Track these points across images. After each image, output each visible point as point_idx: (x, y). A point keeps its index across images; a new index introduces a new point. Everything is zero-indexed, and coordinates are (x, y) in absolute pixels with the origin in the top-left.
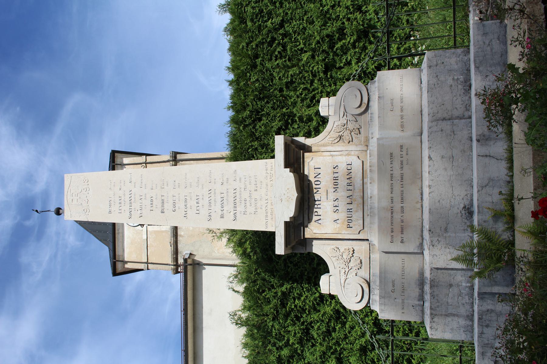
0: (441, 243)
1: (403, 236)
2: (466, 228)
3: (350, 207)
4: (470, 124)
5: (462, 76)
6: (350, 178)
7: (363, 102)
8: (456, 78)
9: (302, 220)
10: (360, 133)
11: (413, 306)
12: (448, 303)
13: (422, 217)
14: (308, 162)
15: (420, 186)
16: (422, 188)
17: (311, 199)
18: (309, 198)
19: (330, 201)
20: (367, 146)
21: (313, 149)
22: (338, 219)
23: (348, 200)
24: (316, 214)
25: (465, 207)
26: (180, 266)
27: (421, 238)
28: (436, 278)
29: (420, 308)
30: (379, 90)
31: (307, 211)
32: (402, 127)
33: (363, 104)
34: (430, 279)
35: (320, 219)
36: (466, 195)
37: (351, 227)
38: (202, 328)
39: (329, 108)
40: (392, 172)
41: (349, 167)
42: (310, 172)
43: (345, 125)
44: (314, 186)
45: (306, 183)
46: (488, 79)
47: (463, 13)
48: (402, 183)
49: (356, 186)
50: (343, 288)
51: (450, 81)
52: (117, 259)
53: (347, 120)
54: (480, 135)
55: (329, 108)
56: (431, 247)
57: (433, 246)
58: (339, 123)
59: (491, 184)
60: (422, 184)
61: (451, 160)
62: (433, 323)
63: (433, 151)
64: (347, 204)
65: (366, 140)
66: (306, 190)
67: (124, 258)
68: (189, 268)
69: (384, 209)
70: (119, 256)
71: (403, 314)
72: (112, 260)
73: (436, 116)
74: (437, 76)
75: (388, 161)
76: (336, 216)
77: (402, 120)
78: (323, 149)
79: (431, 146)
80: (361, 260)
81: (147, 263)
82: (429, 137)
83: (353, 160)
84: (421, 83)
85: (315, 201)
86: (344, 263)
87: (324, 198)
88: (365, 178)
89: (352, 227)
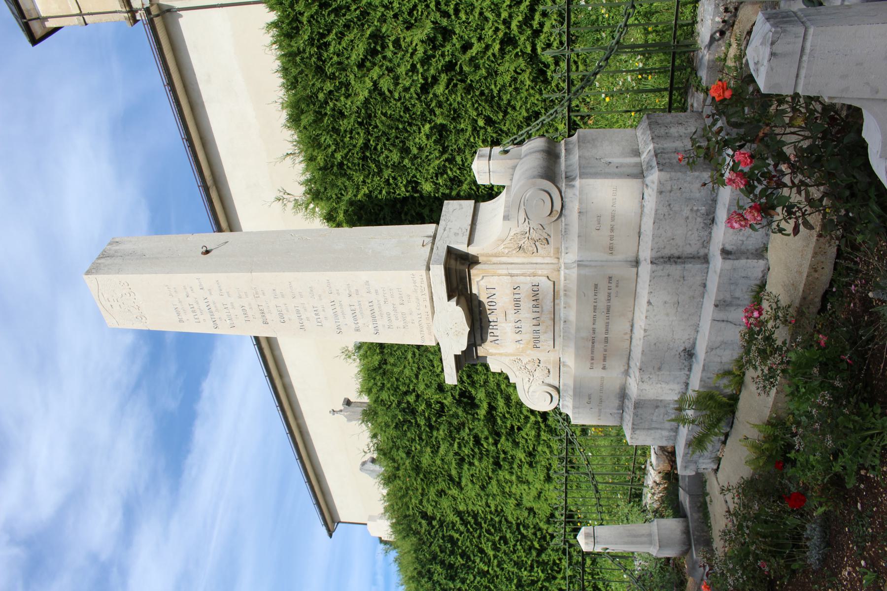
1: (605, 363)
2: (683, 366)
3: (537, 328)
4: (706, 270)
5: (703, 208)
8: (695, 208)
12: (652, 420)
13: (630, 346)
16: (633, 320)
17: (484, 320)
18: (481, 319)
20: (558, 258)
21: (481, 259)
23: (535, 322)
24: (492, 334)
25: (685, 350)
26: (137, 11)
29: (620, 416)
30: (580, 203)
31: (479, 331)
33: (554, 212)
36: (689, 339)
38: (203, 103)
40: (595, 304)
41: (535, 288)
44: (487, 307)
45: (475, 303)
46: (741, 233)
47: (807, 553)
49: (544, 308)
51: (686, 212)
52: (28, 17)
54: (720, 301)
58: (518, 230)
59: (723, 346)
61: (676, 305)
66: (476, 310)
67: (38, 13)
68: (157, 21)
70: (28, 11)
72: (19, 20)
74: (669, 205)
75: (591, 293)
76: (518, 337)
77: (612, 242)
78: (495, 260)
81: (81, 14)
82: (650, 281)
87: (501, 318)
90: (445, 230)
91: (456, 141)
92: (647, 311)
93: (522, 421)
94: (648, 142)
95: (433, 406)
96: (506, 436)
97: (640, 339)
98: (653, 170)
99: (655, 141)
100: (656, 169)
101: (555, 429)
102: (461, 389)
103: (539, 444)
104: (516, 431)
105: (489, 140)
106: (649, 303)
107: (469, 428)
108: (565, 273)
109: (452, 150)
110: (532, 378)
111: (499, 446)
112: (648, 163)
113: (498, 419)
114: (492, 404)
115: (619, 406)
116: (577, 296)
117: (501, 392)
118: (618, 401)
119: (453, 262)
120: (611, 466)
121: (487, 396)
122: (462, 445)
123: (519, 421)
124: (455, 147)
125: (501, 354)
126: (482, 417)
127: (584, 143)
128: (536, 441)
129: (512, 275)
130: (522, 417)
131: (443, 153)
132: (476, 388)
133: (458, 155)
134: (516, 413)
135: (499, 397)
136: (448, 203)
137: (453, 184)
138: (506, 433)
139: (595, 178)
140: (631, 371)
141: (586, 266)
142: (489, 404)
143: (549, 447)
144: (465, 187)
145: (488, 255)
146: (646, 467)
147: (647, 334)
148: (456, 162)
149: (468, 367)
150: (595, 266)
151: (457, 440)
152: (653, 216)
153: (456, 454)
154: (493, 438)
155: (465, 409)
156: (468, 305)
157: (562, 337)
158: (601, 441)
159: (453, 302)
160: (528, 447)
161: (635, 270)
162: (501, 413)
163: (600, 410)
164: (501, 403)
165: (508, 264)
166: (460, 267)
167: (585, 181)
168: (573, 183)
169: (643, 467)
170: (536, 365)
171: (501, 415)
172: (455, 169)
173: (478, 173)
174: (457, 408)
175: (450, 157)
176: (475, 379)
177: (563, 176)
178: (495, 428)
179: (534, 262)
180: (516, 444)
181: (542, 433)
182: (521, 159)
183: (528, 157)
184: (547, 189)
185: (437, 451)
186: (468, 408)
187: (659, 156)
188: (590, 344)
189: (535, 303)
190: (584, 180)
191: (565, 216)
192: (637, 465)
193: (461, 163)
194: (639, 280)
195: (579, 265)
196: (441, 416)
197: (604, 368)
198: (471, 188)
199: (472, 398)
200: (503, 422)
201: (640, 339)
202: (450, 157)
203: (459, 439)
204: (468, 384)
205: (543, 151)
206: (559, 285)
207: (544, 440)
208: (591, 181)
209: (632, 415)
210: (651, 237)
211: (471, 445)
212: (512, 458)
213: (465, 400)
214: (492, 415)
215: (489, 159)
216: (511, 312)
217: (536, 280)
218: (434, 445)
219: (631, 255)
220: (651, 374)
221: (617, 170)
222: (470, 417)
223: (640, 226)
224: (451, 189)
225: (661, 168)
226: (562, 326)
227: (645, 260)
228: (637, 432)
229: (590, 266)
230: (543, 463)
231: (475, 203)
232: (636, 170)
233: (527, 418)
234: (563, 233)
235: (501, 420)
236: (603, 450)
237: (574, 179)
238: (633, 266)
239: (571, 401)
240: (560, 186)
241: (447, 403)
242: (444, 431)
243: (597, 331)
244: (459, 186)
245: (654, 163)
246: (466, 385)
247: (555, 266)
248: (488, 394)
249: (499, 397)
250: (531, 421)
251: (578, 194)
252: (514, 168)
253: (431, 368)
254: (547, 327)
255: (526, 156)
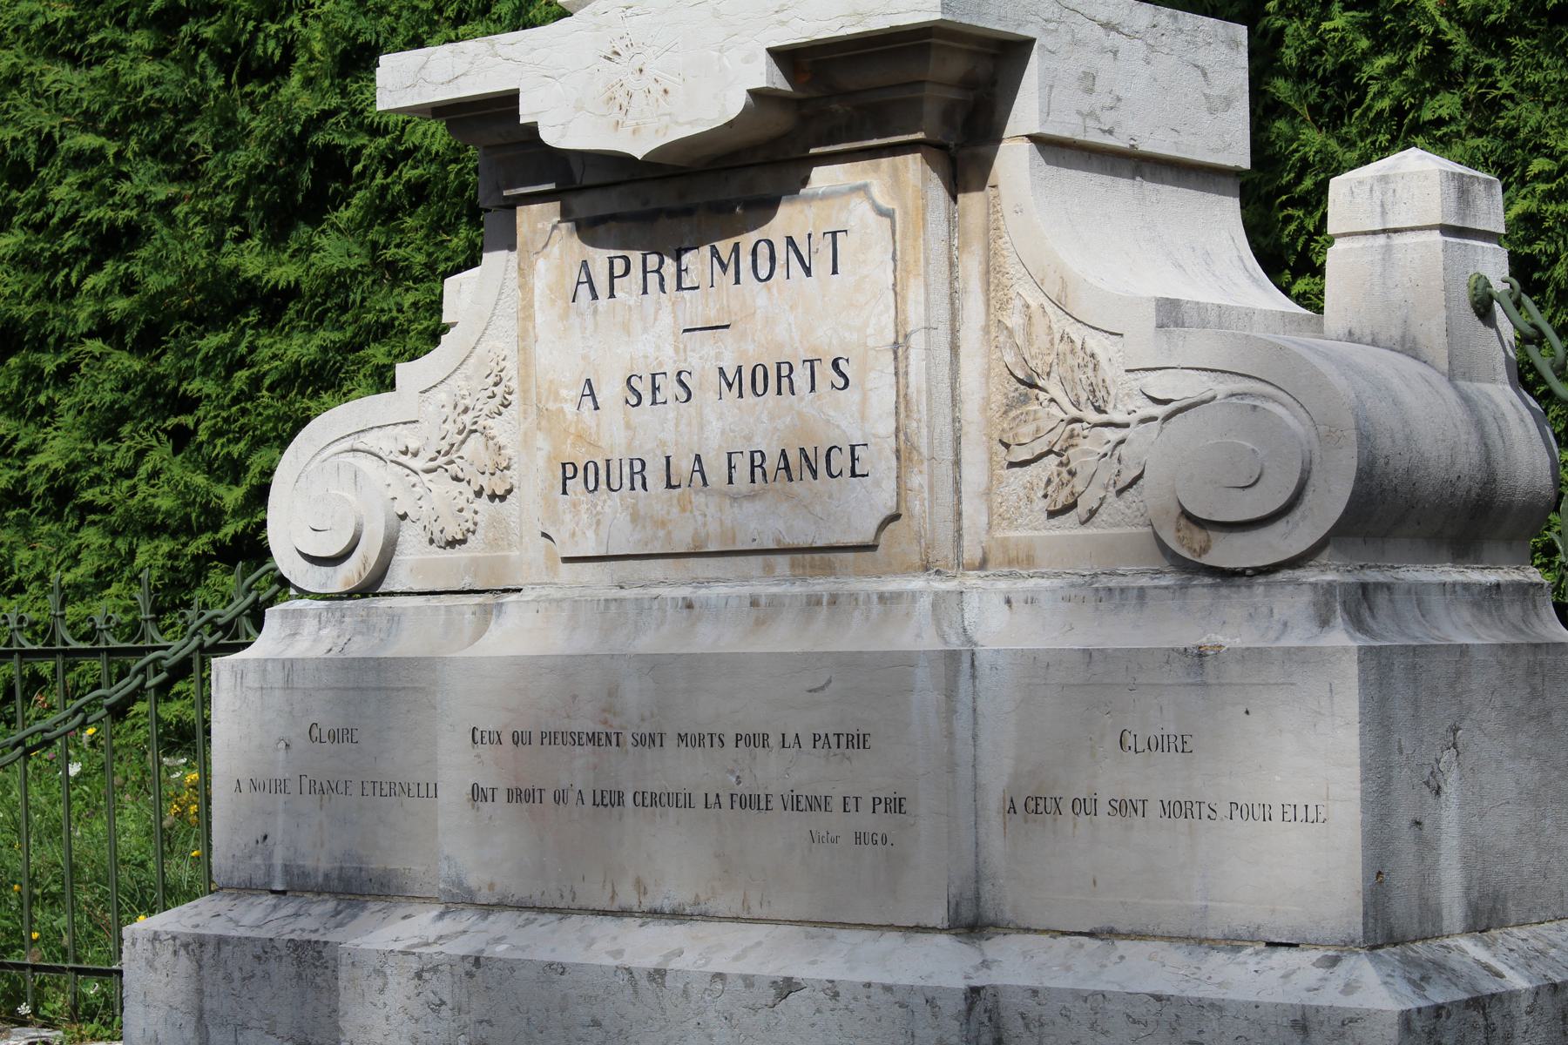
0: (431, 1016)
1: (501, 796)
6: (787, 468)
7: (1213, 534)
9: (586, 182)
10: (1052, 514)
11: (265, 837)
12: (244, 1026)
14: (863, 189)
15: (714, 906)
16: (706, 917)
18: (688, 212)
19: (677, 350)
20: (983, 564)
21: (972, 201)
22: (597, 408)
23: (683, 466)
24: (619, 269)
27: (494, 901)
28: (329, 972)
29: (259, 877)
30: (1248, 656)
31: (635, 206)
32: (1032, 804)
33: (1199, 536)
34: (326, 943)
35: (595, 297)
37: (564, 485)
39: (1374, 233)
40: (774, 741)
41: (841, 461)
42: (816, 205)
43: (1099, 410)
44: (747, 240)
45: (765, 183)
48: (725, 800)
49: (748, 507)
50: (346, 444)
53: (1127, 425)
55: (1374, 233)
56: (415, 965)
57: (419, 975)
58: (1111, 372)
60: (721, 919)
62: (171, 949)
63: (818, 1011)
64: (668, 458)
65: (1013, 554)
69: (610, 694)
71: (235, 784)
73: (1026, 1035)
75: (823, 720)
76: (611, 391)
78: (971, 267)
79: (845, 997)
80: (463, 541)
82: (888, 989)
83: (877, 483)
84: (1270, 944)
85: (678, 259)
86: (444, 446)
87: (698, 308)
88: (793, 566)
89: (564, 492)
90: (1108, 26)
91: (1534, 88)
92: (749, 981)
93: (219, 448)
94: (1539, 968)
95: (273, 28)
96: (143, 373)
97: (619, 953)
98: (1406, 989)
99: (1545, 1000)
100: (1413, 1002)
101: (188, 605)
102: (356, 153)
103: (115, 533)
104: (171, 422)
105: (1539, 246)
106: (786, 988)
107: (172, 202)
108: (914, 596)
109: (1488, 70)
110: (418, 464)
111: (95, 346)
112: (1440, 967)
113: (225, 338)
114: (293, 308)
115: (305, 875)
116: (806, 656)
117: (353, 346)
118: (324, 865)
119: (955, 67)
120: (20, 867)
121: (330, 278)
122: (93, 172)
123: (216, 433)
124: (1505, 86)
125: (526, 313)
126: (229, 262)
127: (1531, 672)
128: (128, 519)
129: (898, 348)
130: (237, 449)
131: (1475, 26)
132: (364, 225)
133: (1466, 104)
134: (252, 419)
135: (325, 336)
136: (1233, 44)
137: (1324, 82)
138: (161, 378)
139: (1364, 723)
140: (467, 919)
141: (951, 692)
142: (292, 292)
143: (102, 580)
144: (1313, 139)
145: (991, 232)
146: (23, 1022)
147: (644, 983)
148: (1434, 93)
149: (464, 186)
150: (950, 735)
151: (112, 148)
152: (1192, 993)
153: (48, 144)
154: (130, 316)
155: (261, 178)
156: (753, 148)
157: (616, 593)
158: (137, 818)
159: (765, 75)
160: (96, 481)
161: (939, 916)
162: (252, 349)
163: (280, 786)
164: (300, 347)
165: (954, 332)
166: (934, 101)
167: (1349, 673)
168: (1339, 619)
169: (24, 1009)
170: (484, 481)
171: (242, 348)
172: (1396, 87)
173: (1384, 179)
174: (264, 140)
175: (1457, 64)
176: (409, 222)
177: (1372, 576)
178: (182, 326)
179: (966, 455)
180: (108, 425)
181: (166, 546)
182: (1451, 378)
183: (1459, 412)
184: (1309, 497)
185: (53, 54)
186: (269, 192)
187: (1476, 1016)
188: (590, 727)
189: (772, 462)
190: (1354, 670)
191: (1183, 587)
192: (30, 981)
193: (1427, 115)
194: (892, 940)
195: (952, 657)
196: (224, 63)
197: (478, 794)
198: (1305, 167)
199: (316, 209)
200: (208, 361)
201: (619, 953)
202: (1457, 64)
203: (119, 156)
204: (384, 189)
205: (1490, 480)
206: (864, 573)
207: (132, 554)
208: (1349, 703)
209: (264, 934)
210: (1091, 986)
211: (94, 214)
212: (40, 410)
213: (306, 178)
214: (240, 308)
215: (1446, 230)
216: (729, 352)
217: (881, 462)
218: (82, 37)
219: (1005, 898)
220: (458, 1009)
221: (1403, 821)
222: (228, 201)
223: (1140, 936)
224: (1301, 75)
225: (1417, 1024)
226: (665, 591)
227: (985, 964)
228: (184, 963)
229: (951, 711)
230: (23, 555)
231: (1235, 173)
232: (1402, 909)
233: (234, 470)
234: (1104, 581)
235: (220, 350)
236: (98, 826)
237: (1357, 623)
238: (954, 909)
239: (320, 652)
240: (1324, 558)
241: (285, 93)
242: (155, 82)
243: (650, 753)
244: (1315, 110)
245: (1438, 994)
246: (379, 180)
247: (945, 551)
248: (337, 283)
249: (325, 336)
250: (220, 489)
251: (1285, 643)
252: (1409, 348)
253: (450, 12)
254: (663, 524)
255: (1466, 399)
